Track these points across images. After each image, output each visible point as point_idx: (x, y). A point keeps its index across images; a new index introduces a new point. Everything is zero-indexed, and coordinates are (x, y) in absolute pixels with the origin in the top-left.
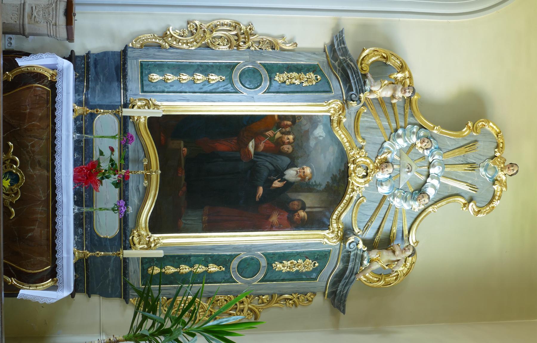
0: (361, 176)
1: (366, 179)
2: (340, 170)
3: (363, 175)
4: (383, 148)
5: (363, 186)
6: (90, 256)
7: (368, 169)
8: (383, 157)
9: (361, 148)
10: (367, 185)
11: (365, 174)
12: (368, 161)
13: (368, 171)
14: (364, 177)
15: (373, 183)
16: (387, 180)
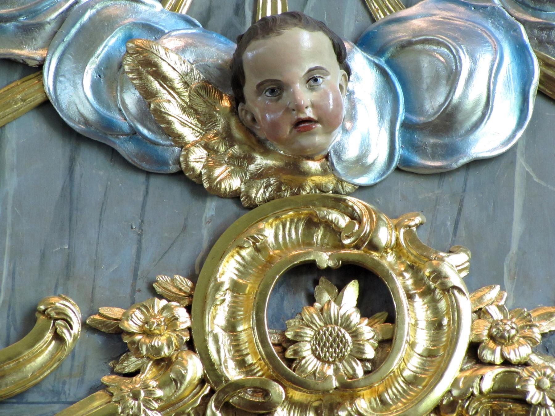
0: (368, 332)
1: (402, 283)
2: (345, 131)
3: (365, 307)
4: (108, 126)
5: (466, 304)
6: (527, 162)
7: (310, 267)
8: (187, 129)
9: (114, 341)
10: (454, 266)
11: (352, 290)
12: (228, 269)
13: (325, 259)
14: (378, 301)
15: (429, 208)
16: (398, 65)
